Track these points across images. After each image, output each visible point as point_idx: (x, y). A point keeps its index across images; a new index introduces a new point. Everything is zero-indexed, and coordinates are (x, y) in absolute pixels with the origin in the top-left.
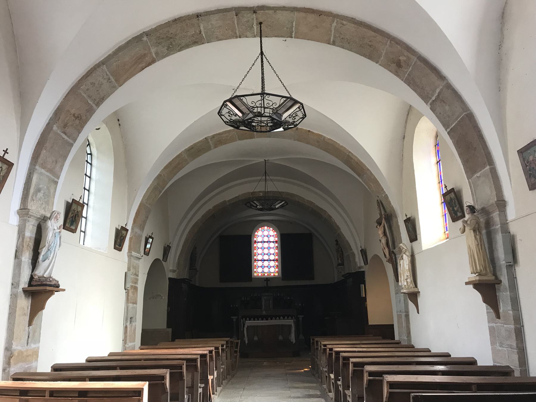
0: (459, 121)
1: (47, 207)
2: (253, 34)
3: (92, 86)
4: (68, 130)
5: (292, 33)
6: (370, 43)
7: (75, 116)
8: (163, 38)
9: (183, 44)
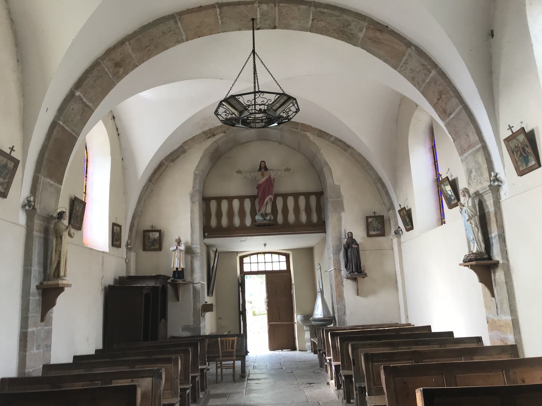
0: (72, 134)
1: (482, 178)
2: (260, 8)
3: (415, 80)
4: (448, 111)
5: (220, 13)
6: (148, 48)
7: (439, 98)
8: (347, 36)
9: (334, 18)
